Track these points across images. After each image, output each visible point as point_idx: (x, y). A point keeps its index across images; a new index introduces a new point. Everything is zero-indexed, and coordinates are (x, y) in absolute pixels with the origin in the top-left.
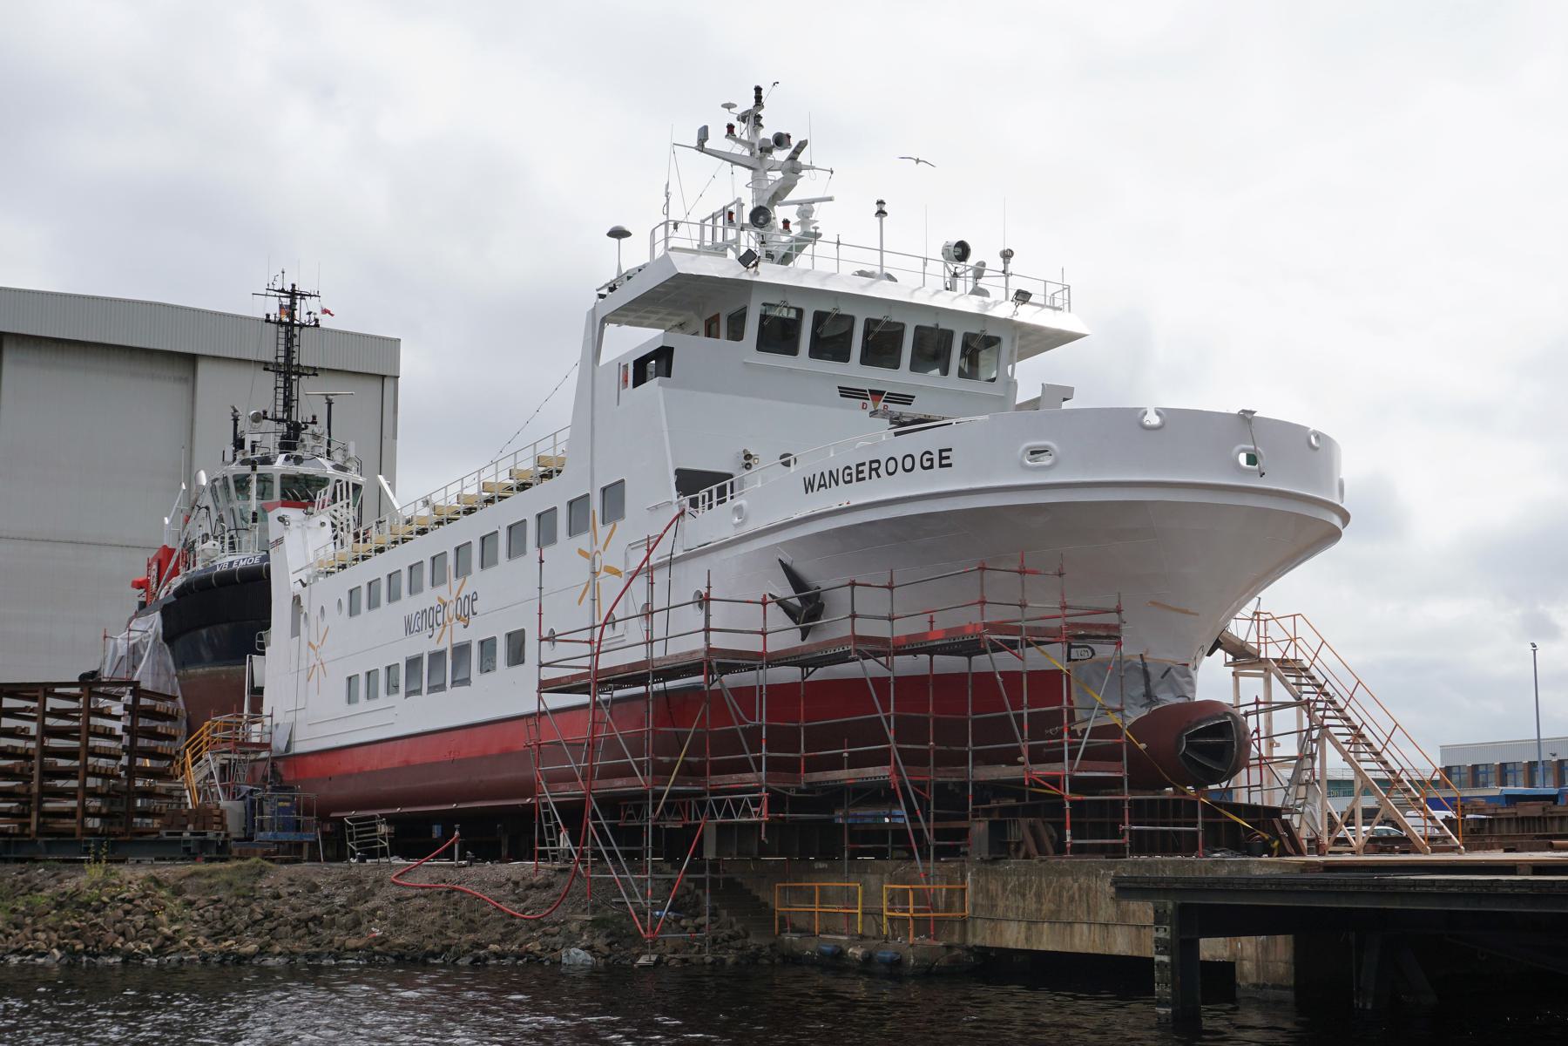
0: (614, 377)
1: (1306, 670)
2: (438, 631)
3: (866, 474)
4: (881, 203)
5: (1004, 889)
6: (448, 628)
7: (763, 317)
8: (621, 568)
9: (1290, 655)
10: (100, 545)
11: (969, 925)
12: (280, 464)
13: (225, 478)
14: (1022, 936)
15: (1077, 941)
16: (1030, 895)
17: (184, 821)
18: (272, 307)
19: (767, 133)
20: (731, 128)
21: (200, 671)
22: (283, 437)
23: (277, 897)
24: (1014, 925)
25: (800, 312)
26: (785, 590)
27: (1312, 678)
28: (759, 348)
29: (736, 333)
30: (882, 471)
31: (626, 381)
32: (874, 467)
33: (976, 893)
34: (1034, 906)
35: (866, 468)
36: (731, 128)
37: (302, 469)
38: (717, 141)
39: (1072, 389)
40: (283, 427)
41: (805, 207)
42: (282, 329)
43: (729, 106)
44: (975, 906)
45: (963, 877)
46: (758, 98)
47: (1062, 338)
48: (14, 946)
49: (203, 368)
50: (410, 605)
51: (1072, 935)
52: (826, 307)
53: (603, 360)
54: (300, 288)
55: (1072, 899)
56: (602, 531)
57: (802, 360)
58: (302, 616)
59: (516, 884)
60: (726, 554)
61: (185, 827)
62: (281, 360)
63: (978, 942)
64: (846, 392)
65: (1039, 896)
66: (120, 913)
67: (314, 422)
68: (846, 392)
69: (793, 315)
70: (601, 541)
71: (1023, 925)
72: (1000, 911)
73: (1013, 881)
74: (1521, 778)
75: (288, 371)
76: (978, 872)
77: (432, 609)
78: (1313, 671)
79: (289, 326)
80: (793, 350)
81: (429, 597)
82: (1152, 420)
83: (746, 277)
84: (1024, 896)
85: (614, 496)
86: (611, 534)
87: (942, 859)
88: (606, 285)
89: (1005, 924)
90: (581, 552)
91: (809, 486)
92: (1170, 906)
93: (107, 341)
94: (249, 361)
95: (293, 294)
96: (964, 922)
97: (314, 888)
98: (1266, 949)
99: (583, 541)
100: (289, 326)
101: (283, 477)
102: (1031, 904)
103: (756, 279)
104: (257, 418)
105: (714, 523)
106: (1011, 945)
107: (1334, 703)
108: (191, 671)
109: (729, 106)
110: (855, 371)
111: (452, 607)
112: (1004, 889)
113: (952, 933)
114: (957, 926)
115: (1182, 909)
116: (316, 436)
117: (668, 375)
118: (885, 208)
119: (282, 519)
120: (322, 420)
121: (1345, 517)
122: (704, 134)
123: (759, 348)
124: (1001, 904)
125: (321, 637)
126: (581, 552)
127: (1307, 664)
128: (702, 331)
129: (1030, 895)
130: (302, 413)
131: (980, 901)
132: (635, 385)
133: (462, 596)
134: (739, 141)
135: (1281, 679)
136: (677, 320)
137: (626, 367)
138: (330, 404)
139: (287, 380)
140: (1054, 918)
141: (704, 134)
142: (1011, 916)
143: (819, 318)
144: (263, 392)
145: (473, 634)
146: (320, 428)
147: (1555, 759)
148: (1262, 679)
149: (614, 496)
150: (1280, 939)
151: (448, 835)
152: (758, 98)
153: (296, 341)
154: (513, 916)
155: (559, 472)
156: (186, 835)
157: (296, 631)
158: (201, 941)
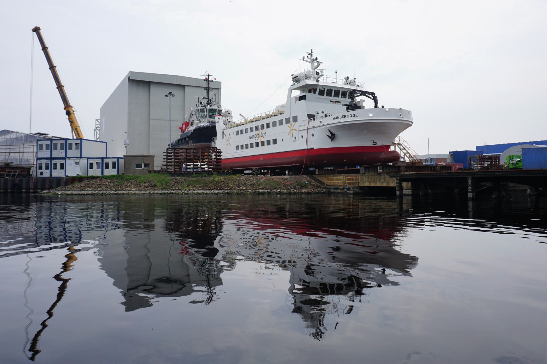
0: (294, 100)
1: (401, 145)
2: (257, 138)
3: (344, 117)
4: (336, 71)
5: (365, 178)
6: (259, 138)
7: (319, 90)
8: (297, 129)
9: (399, 142)
10: (161, 120)
11: (359, 183)
12: (208, 107)
13: (198, 109)
14: (368, 184)
15: (377, 185)
16: (370, 179)
17: (225, 169)
18: (204, 78)
19: (314, 57)
20: (308, 56)
21: (198, 144)
22: (207, 102)
23: (244, 181)
24: (367, 183)
25: (325, 89)
26: (330, 135)
27: (402, 146)
28: (319, 95)
29: (315, 93)
30: (346, 117)
31: (297, 100)
32: (345, 116)
33: (360, 178)
34: (370, 180)
35: (344, 116)
36: (308, 56)
37: (212, 107)
38: (306, 59)
39: (365, 100)
40: (207, 100)
41: (322, 70)
42: (207, 82)
43: (307, 53)
44: (360, 180)
45: (358, 176)
46: (312, 51)
47: (324, 75)
48: (207, 188)
49: (186, 88)
50: (250, 134)
51: (377, 184)
52: (329, 88)
53: (292, 96)
54: (210, 74)
55: (377, 179)
56: (293, 124)
57: (325, 97)
58: (225, 135)
59: (282, 179)
60: (318, 128)
61: (225, 170)
62: (207, 87)
63: (361, 185)
64: (331, 101)
65: (371, 179)
66: (222, 183)
67: (213, 99)
68: (331, 101)
69: (323, 89)
70: (293, 125)
71: (368, 183)
72: (365, 181)
73: (367, 177)
74: (429, 162)
75: (208, 89)
76: (361, 176)
77: (256, 135)
78: (403, 145)
79: (207, 80)
80: (323, 95)
81: (255, 132)
82: (387, 110)
83: (317, 84)
84: (369, 179)
85: (295, 119)
86: (295, 124)
87: (331, 175)
88: (509, 159)
89: (365, 183)
90: (288, 126)
91: (334, 118)
92: (398, 178)
93: (162, 82)
94: (200, 87)
95: (209, 76)
96: (358, 183)
97: (250, 180)
98: (407, 184)
99: (289, 125)
100: (207, 80)
101: (209, 109)
102: (370, 180)
103: (318, 84)
104: (204, 98)
105: (313, 124)
106: (366, 186)
107: (406, 150)
108: (197, 144)
109: (307, 53)
110: (333, 98)
111: (260, 135)
112: (365, 178)
113: (356, 184)
114: (357, 183)
115: (400, 178)
116: (213, 101)
117: (305, 99)
118: (337, 72)
119: (219, 118)
120: (214, 98)
121: (413, 123)
122: (304, 58)
123: (319, 95)
124: (365, 180)
125: (229, 139)
126: (288, 126)
127: (401, 144)
128: (308, 92)
129: (370, 179)
130: (211, 97)
131: (361, 179)
132: (299, 101)
133: (262, 133)
134: (309, 59)
135: (398, 146)
136: (303, 90)
137: (297, 98)
138: (215, 95)
139: (208, 91)
140: (374, 182)
141: (304, 58)
142: (366, 181)
143: (328, 90)
144: (204, 93)
145: (265, 139)
146: (213, 100)
147: (430, 158)
148: (394, 146)
149: (295, 119)
150: (409, 183)
151: (268, 171)
152: (312, 51)
153: (209, 84)
154: (283, 184)
155: (283, 113)
156: (226, 172)
157: (223, 137)
158: (236, 187)
